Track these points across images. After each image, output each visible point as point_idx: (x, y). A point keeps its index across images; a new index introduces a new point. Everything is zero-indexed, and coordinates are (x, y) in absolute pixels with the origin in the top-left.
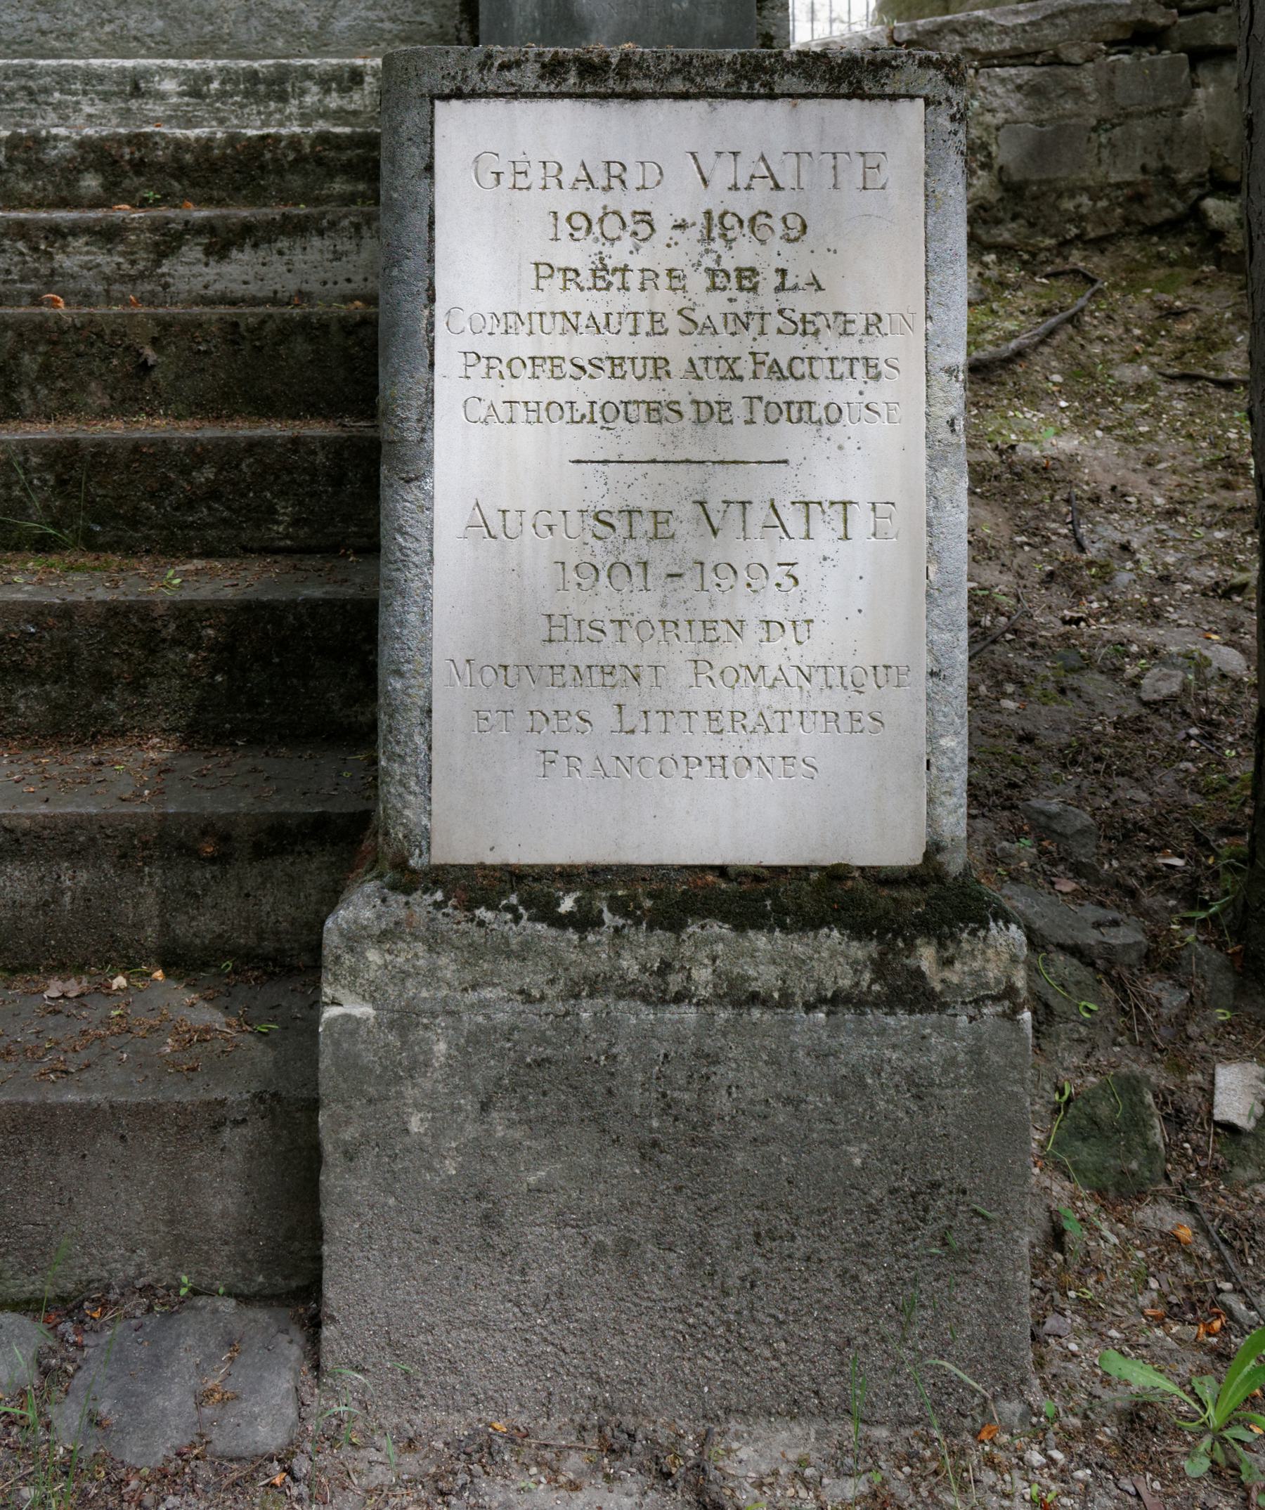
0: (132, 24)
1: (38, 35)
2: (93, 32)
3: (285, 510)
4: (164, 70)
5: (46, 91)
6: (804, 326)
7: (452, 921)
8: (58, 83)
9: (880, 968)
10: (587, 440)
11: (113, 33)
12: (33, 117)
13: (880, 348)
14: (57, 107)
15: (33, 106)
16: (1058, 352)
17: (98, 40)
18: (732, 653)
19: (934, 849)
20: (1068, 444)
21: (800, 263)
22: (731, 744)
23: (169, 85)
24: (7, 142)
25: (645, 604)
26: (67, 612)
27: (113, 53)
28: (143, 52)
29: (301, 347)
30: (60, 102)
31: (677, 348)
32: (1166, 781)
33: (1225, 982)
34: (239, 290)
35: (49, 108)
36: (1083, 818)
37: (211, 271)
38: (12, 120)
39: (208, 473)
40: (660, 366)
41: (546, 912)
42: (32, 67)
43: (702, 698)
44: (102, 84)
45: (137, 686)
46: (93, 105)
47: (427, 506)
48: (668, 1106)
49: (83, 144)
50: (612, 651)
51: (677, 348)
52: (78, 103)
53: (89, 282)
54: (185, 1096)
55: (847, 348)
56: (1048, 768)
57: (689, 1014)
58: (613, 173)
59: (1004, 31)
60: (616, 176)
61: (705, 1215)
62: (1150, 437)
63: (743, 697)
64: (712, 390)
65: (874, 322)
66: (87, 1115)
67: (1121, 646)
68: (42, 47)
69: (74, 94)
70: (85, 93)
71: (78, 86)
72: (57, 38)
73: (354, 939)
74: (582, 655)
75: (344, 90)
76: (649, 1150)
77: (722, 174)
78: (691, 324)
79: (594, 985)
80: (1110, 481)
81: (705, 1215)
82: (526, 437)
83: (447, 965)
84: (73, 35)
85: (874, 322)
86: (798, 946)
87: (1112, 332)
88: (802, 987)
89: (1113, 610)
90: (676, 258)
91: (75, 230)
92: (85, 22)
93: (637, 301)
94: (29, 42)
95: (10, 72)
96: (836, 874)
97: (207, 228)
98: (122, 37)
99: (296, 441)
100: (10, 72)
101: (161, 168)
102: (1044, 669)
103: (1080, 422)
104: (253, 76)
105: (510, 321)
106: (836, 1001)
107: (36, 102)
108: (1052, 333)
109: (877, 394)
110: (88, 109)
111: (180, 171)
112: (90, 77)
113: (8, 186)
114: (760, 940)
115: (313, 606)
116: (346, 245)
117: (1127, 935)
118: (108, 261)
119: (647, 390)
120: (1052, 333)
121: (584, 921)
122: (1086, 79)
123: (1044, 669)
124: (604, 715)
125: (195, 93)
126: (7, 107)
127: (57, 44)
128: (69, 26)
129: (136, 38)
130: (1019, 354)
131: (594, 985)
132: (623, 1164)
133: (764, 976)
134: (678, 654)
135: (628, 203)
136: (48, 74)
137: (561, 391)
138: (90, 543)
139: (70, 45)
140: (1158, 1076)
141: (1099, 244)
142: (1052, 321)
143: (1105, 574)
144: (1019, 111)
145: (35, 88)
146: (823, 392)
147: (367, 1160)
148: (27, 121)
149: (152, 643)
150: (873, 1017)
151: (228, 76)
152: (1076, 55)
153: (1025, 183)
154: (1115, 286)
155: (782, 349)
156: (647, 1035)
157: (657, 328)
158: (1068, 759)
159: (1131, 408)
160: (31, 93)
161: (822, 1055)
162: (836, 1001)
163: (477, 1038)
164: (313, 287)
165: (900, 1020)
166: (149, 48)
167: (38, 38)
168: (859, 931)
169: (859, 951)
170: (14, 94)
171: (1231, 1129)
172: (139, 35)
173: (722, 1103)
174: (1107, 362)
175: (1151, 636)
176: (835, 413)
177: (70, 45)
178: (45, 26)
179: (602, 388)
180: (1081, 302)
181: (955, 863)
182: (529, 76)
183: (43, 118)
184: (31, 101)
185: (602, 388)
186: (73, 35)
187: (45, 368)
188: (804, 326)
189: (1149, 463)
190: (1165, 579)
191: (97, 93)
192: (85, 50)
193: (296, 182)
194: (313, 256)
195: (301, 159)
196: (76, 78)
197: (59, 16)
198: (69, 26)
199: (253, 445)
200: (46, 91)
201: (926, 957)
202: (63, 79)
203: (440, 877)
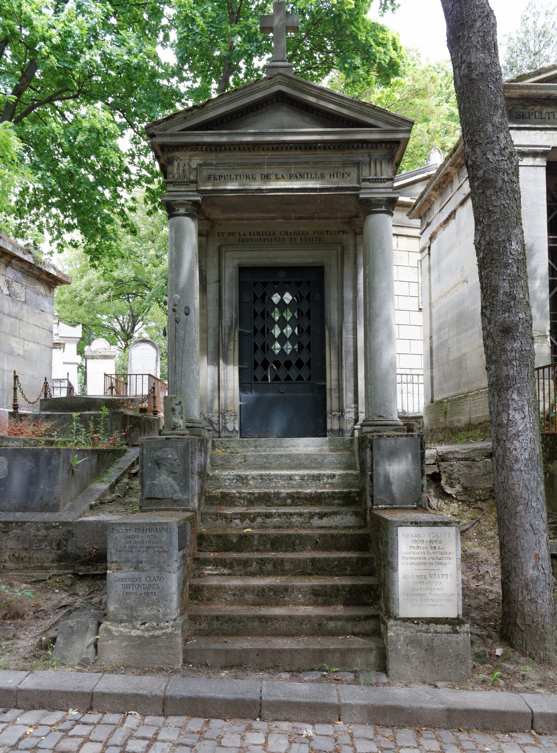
3: (349, 569)
4: (296, 475)
6: (442, 553)
7: (403, 624)
9: (452, 629)
10: (417, 567)
13: (451, 556)
14: (275, 482)
16: (475, 528)
18: (434, 592)
19: (458, 615)
20: (477, 550)
21: (441, 546)
22: (434, 603)
23: (297, 478)
25: (424, 586)
26: (325, 586)
29: (344, 539)
31: (427, 556)
32: (491, 612)
33: (499, 639)
34: (325, 525)
36: (478, 617)
37: (320, 521)
39: (336, 563)
40: (425, 558)
41: (413, 623)
43: (431, 597)
45: (336, 597)
47: (398, 575)
48: (428, 645)
49: (288, 494)
50: (420, 592)
51: (427, 556)
53: (297, 524)
54: (368, 647)
55: (447, 556)
56: (473, 610)
57: (431, 634)
59: (462, 453)
60: (419, 536)
61: (433, 658)
62: (493, 548)
63: (435, 597)
64: (431, 561)
65: (450, 553)
66: (356, 649)
67: (486, 590)
73: (392, 626)
74: (416, 592)
75: (332, 479)
76: (426, 650)
77: (432, 536)
78: (428, 553)
79: (420, 631)
80: (485, 558)
81: (433, 658)
82: (409, 566)
83: (402, 629)
85: (450, 553)
86: (443, 626)
87: (486, 524)
88: (443, 631)
89: (485, 583)
90: (426, 545)
91: (295, 514)
93: (422, 550)
96: (447, 618)
97: (319, 514)
99: (350, 557)
101: (302, 498)
102: (473, 594)
103: (480, 545)
104: (313, 476)
105: (407, 553)
106: (448, 633)
108: (474, 524)
109: (451, 561)
111: (306, 499)
112: (281, 476)
114: (438, 626)
115: (362, 585)
116: (344, 517)
117: (485, 633)
118: (301, 520)
119: (424, 561)
120: (474, 524)
121: (418, 624)
122: (480, 464)
123: (473, 594)
124: (419, 600)
125: (302, 479)
130: (467, 529)
131: (420, 631)
132: (423, 652)
133: (439, 630)
134: (428, 592)
135: (421, 539)
137: (413, 561)
138: (317, 574)
140: (488, 650)
141: (484, 501)
142: (474, 521)
143: (484, 577)
144: (466, 471)
146: (444, 561)
147: (394, 651)
149: (338, 590)
150: (452, 635)
151: (308, 475)
152: (478, 459)
153: (468, 487)
154: (487, 512)
155: (439, 556)
156: (426, 637)
157: (424, 554)
158: (476, 609)
159: (490, 541)
161: (446, 639)
162: (448, 633)
163: (406, 637)
164: (338, 524)
165: (455, 635)
168: (450, 625)
169: (450, 627)
171: (498, 656)
173: (435, 645)
174: (485, 531)
175: (491, 588)
176: (445, 564)
179: (418, 561)
180: (480, 516)
181: (461, 617)
182: (409, 524)
185: (418, 561)
187: (300, 542)
188: (442, 553)
189: (493, 554)
190: (494, 578)
193: (328, 501)
194: (338, 519)
195: (329, 496)
199: (343, 558)
201: (458, 628)
202: (276, 476)
203: (400, 619)
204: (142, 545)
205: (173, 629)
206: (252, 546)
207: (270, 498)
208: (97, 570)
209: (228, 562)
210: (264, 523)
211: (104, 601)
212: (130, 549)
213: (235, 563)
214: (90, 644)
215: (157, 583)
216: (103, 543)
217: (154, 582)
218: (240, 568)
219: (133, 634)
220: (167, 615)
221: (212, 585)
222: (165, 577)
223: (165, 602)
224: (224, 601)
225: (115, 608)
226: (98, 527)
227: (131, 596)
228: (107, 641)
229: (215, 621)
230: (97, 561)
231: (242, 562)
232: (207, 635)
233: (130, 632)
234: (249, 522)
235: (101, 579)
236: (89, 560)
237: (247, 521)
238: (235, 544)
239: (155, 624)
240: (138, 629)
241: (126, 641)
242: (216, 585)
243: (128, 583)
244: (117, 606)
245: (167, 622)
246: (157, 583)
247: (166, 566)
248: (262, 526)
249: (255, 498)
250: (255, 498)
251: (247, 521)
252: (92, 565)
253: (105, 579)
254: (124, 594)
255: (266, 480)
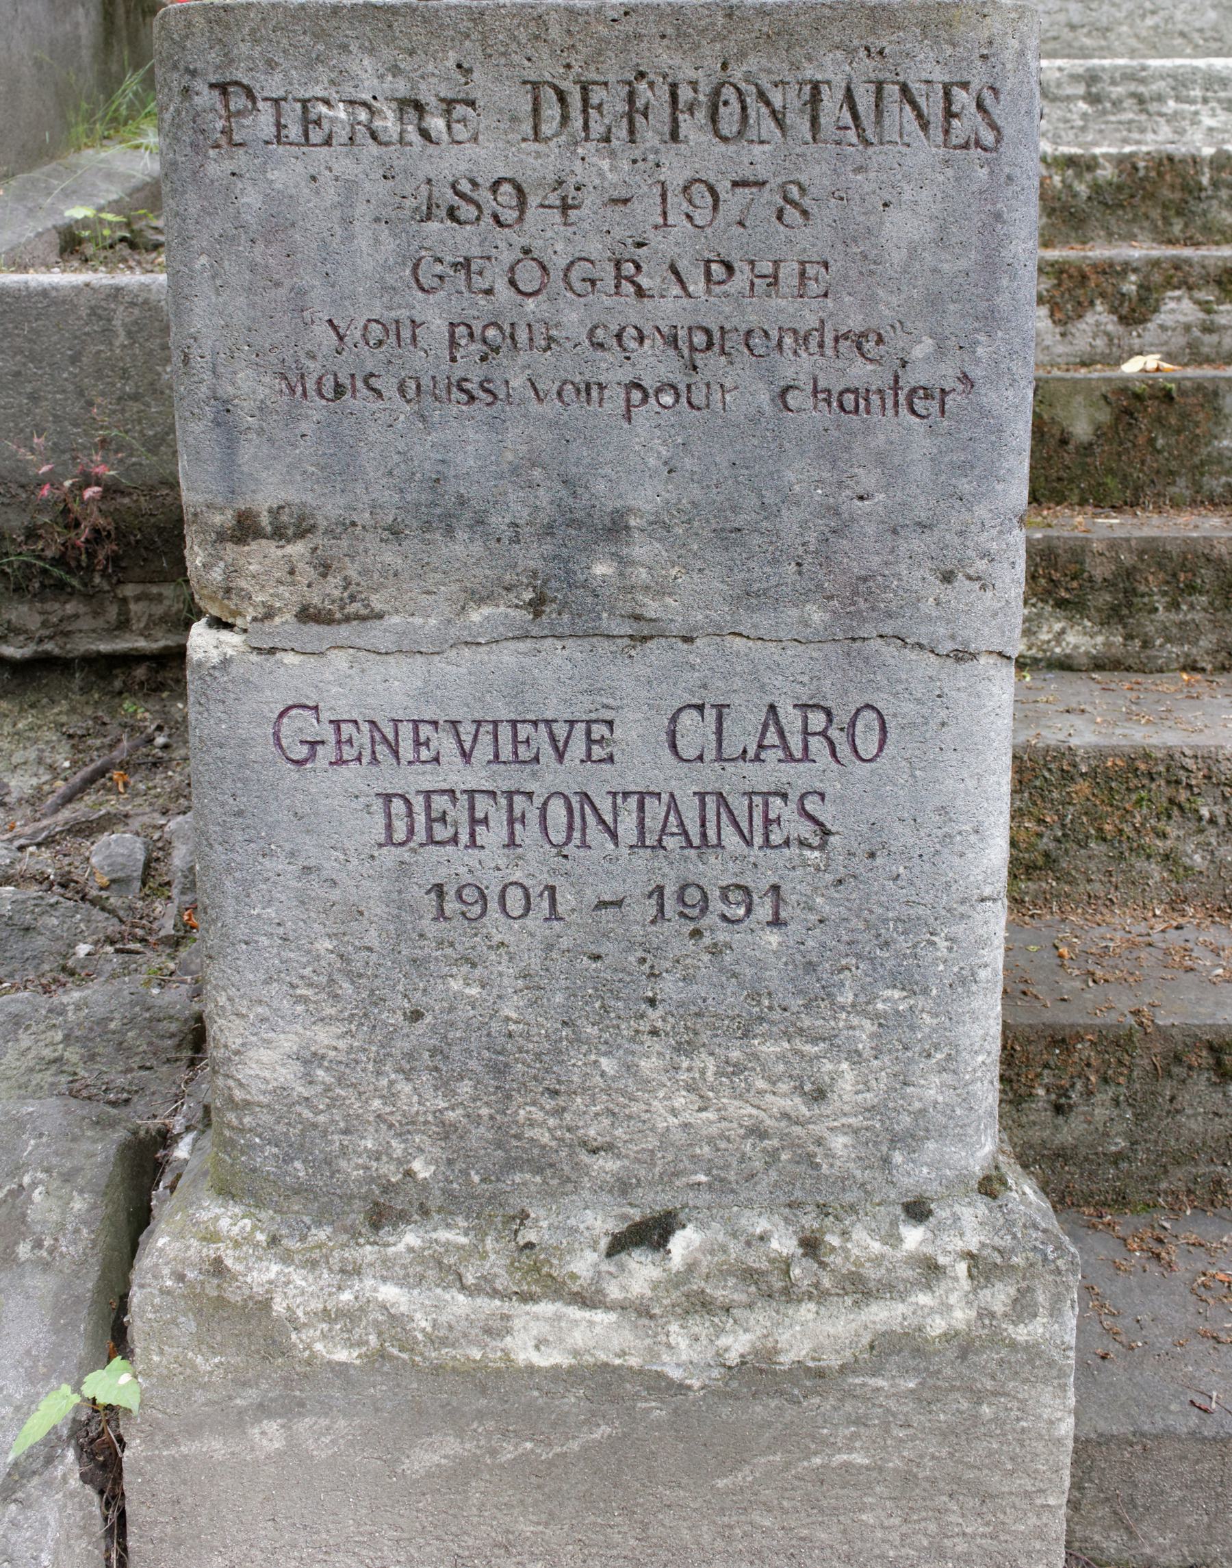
0: (1179, 15)
1: (1066, 30)
2: (1131, 26)
5: (1160, 98)
8: (1173, 89)
11: (1156, 28)
12: (1142, 131)
14: (1172, 118)
15: (1143, 117)
17: (1137, 36)
24: (1211, 162)
27: (1153, 52)
28: (1188, 51)
30: (1176, 113)
35: (1162, 120)
38: (1118, 135)
42: (1144, 68)
44: (1225, 90)
46: (1214, 115)
52: (1196, 113)
58: (624, 273)
68: (1070, 46)
69: (1192, 102)
70: (1205, 101)
71: (1197, 93)
72: (1089, 34)
84: (1107, 29)
92: (1123, 14)
94: (1055, 38)
95: (1117, 75)
98: (1165, 33)
100: (1117, 75)
107: (1148, 113)
110: (1208, 121)
113: (1209, 216)
126: (1113, 118)
127: (1088, 42)
128: (1104, 19)
129: (1182, 34)
136: (1162, 78)
139: (1103, 43)
145: (1147, 95)
148: (1136, 136)
160: (1141, 100)
166: (1196, 46)
167: (1067, 34)
170: (1121, 102)
172: (1186, 29)
177: (1103, 43)
178: (1076, 19)
183: (1154, 132)
184: (1141, 111)
186: (1107, 29)
191: (1219, 101)
192: (1121, 49)
196: (1194, 82)
197: (1093, 6)
198: (1104, 19)
200: (1160, 98)
202: (1180, 82)
204: (629, 311)
205: (999, 1297)
206: (1198, 469)
207: (1192, 189)
208: (123, 625)
209: (1100, 570)
210: (1208, 329)
211: (179, 857)
212: (469, 367)
213: (1152, 583)
214: (47, 1452)
215: (798, 777)
216: (153, 449)
217: (761, 776)
218: (1184, 614)
219: (525, 1353)
220: (908, 1140)
221: (1065, 753)
222: (899, 710)
223: (891, 998)
224: (1156, 872)
225: (310, 1060)
226: (107, 333)
227: (496, 926)
228: (238, 1423)
229: (1201, 1082)
230: (119, 569)
231: (1207, 575)
232: (1121, 1201)
233: (497, 1329)
234: (1110, 322)
235: (153, 688)
236: (60, 561)
237: (1100, 316)
238: (1087, 449)
239: (784, 1244)
240: (588, 1299)
241: (455, 1420)
242: (1101, 754)
243: (455, 775)
244: (324, 1037)
245: (917, 1211)
246: (798, 777)
247: (922, 580)
248: (1193, 346)
249: (1096, 188)
250: (1096, 188)
251: (1100, 316)
252: (89, 595)
253: (179, 688)
254: (401, 906)
255: (1117, 104)
